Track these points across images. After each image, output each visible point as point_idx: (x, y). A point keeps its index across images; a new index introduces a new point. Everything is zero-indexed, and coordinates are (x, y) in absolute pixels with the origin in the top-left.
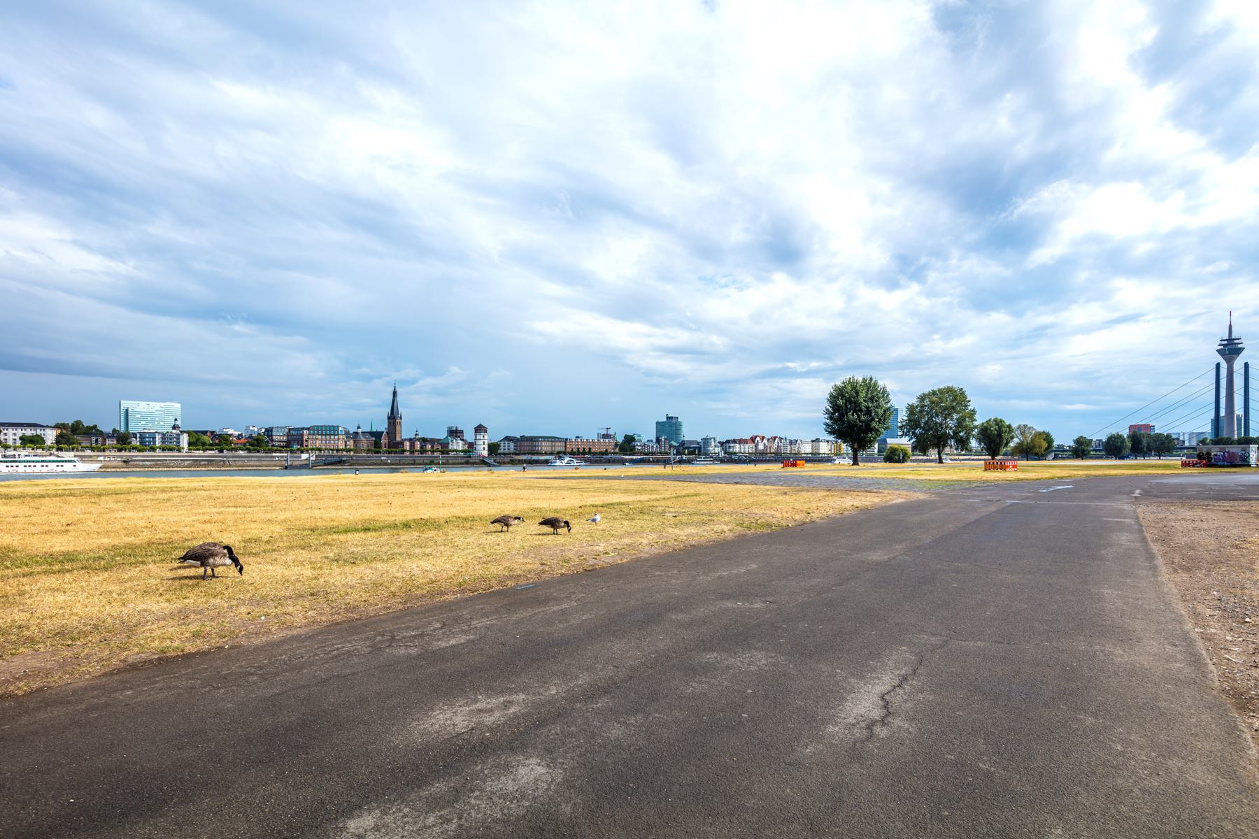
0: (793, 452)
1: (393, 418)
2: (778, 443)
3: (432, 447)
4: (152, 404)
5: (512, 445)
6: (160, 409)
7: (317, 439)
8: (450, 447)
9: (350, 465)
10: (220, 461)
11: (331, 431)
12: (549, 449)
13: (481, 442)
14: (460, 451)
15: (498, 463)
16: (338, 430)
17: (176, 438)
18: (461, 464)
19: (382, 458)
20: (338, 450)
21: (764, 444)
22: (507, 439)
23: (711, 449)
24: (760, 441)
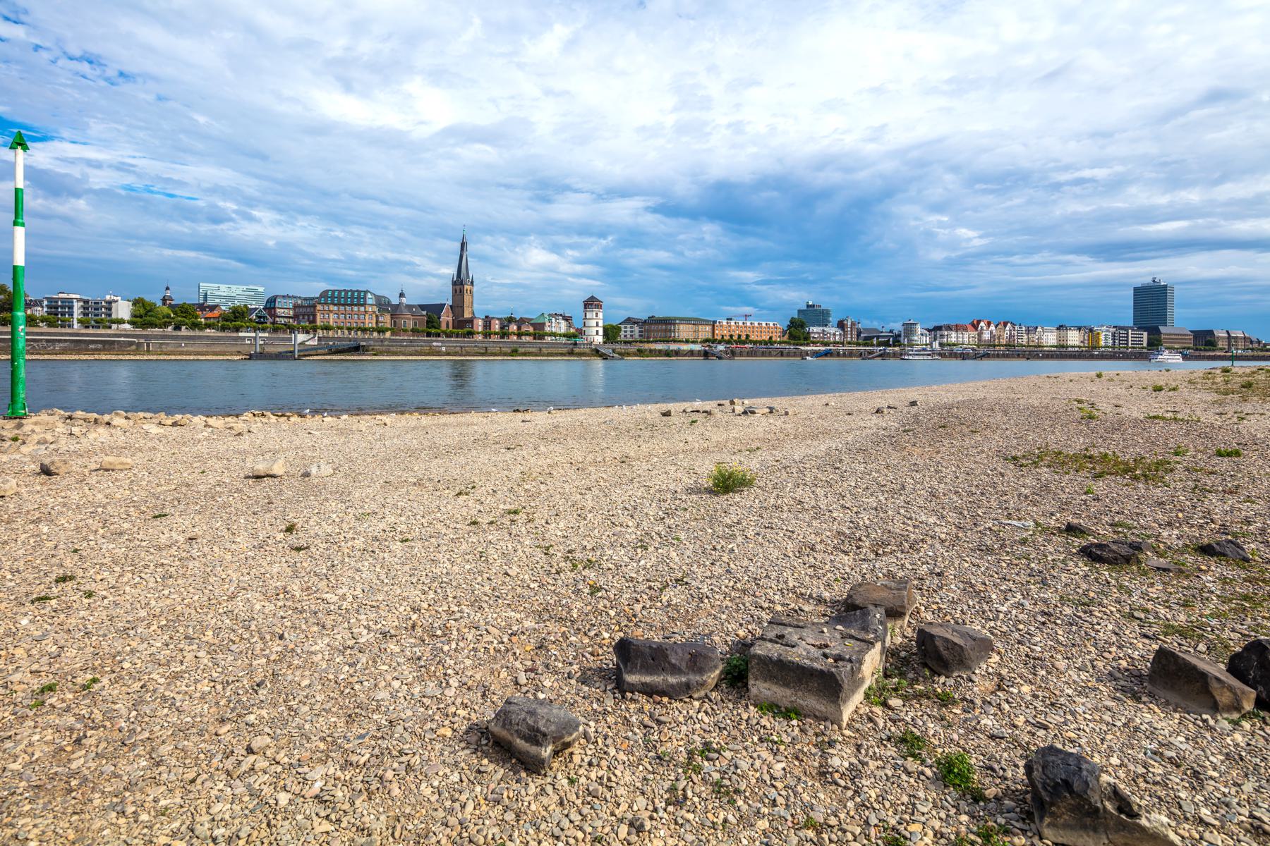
0: (1031, 344)
1: (460, 284)
2: (1010, 330)
3: (519, 328)
4: (234, 287)
5: (636, 329)
6: (241, 293)
7: (331, 311)
8: (547, 329)
9: (375, 355)
10: (131, 343)
11: (353, 299)
12: (691, 336)
13: (593, 323)
14: (560, 335)
15: (620, 354)
16: (365, 298)
17: (106, 308)
18: (562, 354)
19: (435, 344)
20: (364, 330)
21: (991, 332)
22: (629, 321)
23: (916, 338)
24: (985, 328)
